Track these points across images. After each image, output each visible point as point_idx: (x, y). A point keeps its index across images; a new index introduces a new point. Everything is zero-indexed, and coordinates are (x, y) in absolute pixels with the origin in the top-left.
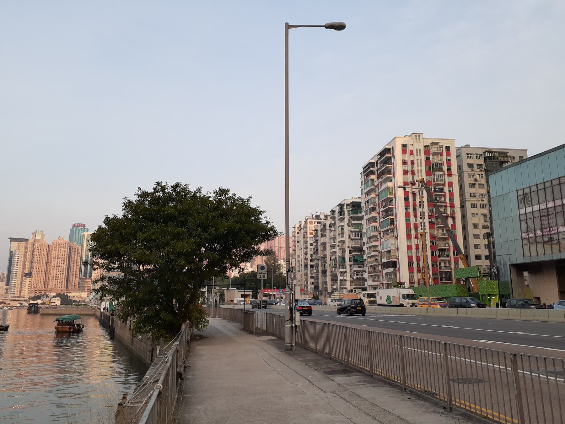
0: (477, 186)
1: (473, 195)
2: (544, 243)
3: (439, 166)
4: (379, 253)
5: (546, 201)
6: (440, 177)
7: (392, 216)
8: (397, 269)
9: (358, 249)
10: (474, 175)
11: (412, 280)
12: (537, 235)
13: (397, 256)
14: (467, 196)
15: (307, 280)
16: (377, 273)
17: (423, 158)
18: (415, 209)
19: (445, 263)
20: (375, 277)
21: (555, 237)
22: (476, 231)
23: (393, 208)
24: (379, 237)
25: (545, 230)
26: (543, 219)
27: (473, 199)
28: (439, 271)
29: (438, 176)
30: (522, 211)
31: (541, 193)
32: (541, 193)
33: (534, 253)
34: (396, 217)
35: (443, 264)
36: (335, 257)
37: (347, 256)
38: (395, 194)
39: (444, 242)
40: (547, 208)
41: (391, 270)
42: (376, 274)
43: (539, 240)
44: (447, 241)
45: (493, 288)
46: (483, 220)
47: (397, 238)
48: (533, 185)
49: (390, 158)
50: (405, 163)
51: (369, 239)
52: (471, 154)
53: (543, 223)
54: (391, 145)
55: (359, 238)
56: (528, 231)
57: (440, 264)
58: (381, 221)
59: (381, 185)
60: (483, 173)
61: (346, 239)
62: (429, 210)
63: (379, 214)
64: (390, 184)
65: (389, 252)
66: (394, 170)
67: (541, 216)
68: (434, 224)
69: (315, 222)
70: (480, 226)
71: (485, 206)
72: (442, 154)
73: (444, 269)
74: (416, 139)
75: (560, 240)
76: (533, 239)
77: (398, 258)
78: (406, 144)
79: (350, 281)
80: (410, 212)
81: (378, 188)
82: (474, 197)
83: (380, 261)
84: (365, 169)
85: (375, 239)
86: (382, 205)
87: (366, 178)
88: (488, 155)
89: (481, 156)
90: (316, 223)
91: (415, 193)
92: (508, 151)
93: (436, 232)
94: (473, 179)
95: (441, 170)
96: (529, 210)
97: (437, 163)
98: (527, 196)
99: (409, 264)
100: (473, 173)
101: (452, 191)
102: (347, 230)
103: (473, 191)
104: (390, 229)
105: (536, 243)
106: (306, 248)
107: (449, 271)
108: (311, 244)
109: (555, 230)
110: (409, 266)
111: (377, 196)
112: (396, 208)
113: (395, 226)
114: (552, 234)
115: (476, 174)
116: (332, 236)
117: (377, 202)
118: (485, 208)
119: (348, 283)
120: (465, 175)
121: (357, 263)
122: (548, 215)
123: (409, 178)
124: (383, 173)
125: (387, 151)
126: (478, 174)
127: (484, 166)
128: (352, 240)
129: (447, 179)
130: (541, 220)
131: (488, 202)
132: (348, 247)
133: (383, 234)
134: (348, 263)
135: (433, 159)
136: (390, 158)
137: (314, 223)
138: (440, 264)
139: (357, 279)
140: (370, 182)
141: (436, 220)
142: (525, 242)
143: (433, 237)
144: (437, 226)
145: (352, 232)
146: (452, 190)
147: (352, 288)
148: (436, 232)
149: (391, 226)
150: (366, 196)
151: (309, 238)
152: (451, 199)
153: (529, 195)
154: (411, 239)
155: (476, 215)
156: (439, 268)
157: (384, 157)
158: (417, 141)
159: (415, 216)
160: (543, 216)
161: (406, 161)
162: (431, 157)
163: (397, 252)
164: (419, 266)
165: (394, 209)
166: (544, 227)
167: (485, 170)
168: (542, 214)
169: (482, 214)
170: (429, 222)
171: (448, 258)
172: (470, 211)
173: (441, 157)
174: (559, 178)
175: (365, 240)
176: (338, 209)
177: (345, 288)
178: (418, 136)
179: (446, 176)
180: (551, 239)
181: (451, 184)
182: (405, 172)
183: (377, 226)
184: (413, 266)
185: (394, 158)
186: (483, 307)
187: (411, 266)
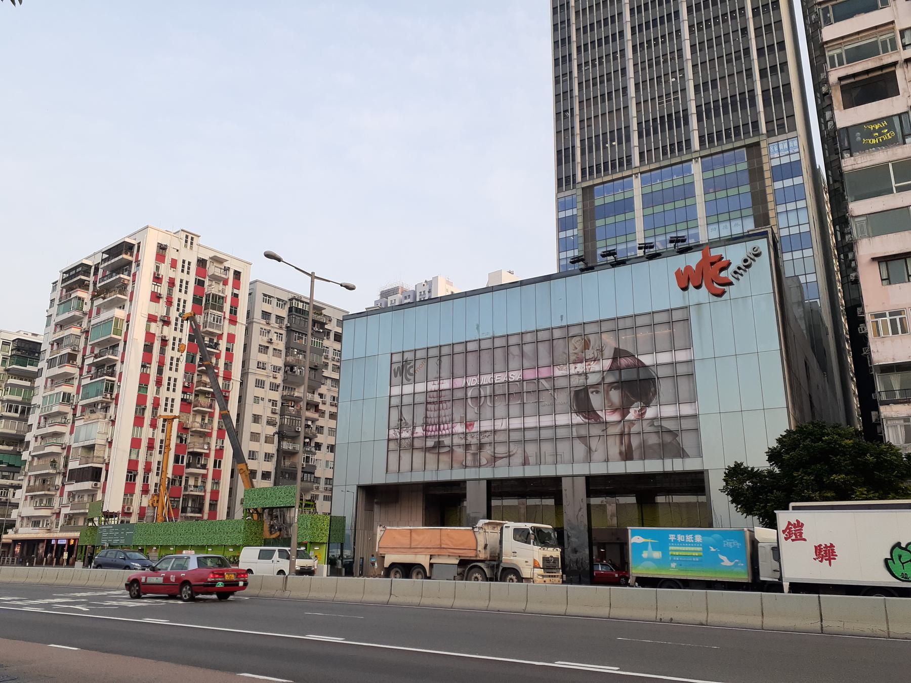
0: (270, 351)
1: (261, 366)
2: (426, 450)
3: (216, 302)
4: (63, 449)
5: (440, 377)
6: (217, 322)
7: (111, 376)
8: (100, 484)
9: (10, 439)
10: (268, 332)
11: (129, 509)
12: (415, 435)
13: (106, 457)
14: (253, 366)
16: (49, 490)
17: (192, 278)
18: (160, 371)
19: (196, 480)
20: (41, 501)
21: (447, 441)
22: (256, 428)
23: (117, 360)
24: (70, 417)
25: (431, 427)
26: (429, 409)
27: (260, 371)
28: (183, 493)
29: (214, 318)
30: (396, 391)
31: (433, 363)
32: (433, 363)
33: (405, 465)
34: (120, 380)
35: (191, 482)
38: (126, 333)
39: (201, 440)
40: (466, 387)
41: (88, 485)
42: (47, 492)
43: (417, 444)
44: (208, 440)
45: (322, 530)
46: (269, 411)
47: (113, 422)
48: (409, 349)
49: (130, 263)
50: (157, 279)
51: (45, 418)
52: (270, 297)
53: (428, 416)
54: (135, 239)
55: (17, 415)
56: (401, 426)
57: (187, 481)
58: (83, 384)
59: (98, 313)
60: (284, 332)
62: (185, 376)
63: (81, 369)
64: (119, 313)
65: (91, 448)
66: (133, 287)
67: (427, 403)
68: (190, 403)
70: (264, 420)
71: (278, 388)
72: (225, 283)
73: (191, 491)
74: (186, 242)
75: (453, 447)
76: (407, 441)
77: (107, 461)
78: (166, 246)
80: (149, 375)
81: (90, 317)
82: (263, 369)
83: (62, 467)
85: (59, 420)
86: (92, 352)
87: (64, 293)
88: (295, 304)
89: (285, 304)
91: (167, 341)
92: (324, 306)
93: (191, 420)
94: (266, 339)
95: (221, 309)
96: (408, 389)
97: (216, 295)
98: (408, 366)
99: (127, 476)
100: (268, 328)
101: (232, 351)
103: (262, 358)
104: (102, 402)
105: (413, 449)
107: (200, 496)
109: (448, 429)
110: (127, 480)
111: (83, 333)
112: (122, 362)
113: (114, 396)
114: (442, 435)
115: (273, 331)
117: (82, 346)
118: (277, 391)
120: (256, 328)
122: (440, 402)
123: (160, 309)
124: (107, 289)
126: (275, 333)
127: (286, 322)
129: (227, 328)
130: (426, 410)
131: (283, 381)
133: (83, 411)
135: (210, 286)
136: (130, 263)
138: (187, 481)
140: (74, 303)
141: (194, 399)
142: (392, 445)
143: (183, 428)
146: (232, 349)
148: (191, 420)
149: (106, 395)
150: (58, 330)
152: (228, 366)
153: (412, 364)
154: (142, 426)
156: (183, 489)
157: (117, 259)
158: (186, 246)
159: (159, 383)
160: (430, 403)
161: (160, 277)
162: (207, 283)
163: (107, 449)
164: (147, 482)
165: (119, 364)
166: (429, 422)
167: (287, 327)
168: (429, 400)
169: (270, 400)
170: (182, 400)
171: (203, 471)
172: (252, 391)
173: (224, 287)
174: (466, 342)
175: (33, 419)
178: (190, 239)
179: (227, 322)
180: (439, 445)
181: (231, 338)
182: (156, 297)
183: (69, 394)
184: (134, 480)
185: (138, 265)
186: (349, 572)
187: (131, 480)
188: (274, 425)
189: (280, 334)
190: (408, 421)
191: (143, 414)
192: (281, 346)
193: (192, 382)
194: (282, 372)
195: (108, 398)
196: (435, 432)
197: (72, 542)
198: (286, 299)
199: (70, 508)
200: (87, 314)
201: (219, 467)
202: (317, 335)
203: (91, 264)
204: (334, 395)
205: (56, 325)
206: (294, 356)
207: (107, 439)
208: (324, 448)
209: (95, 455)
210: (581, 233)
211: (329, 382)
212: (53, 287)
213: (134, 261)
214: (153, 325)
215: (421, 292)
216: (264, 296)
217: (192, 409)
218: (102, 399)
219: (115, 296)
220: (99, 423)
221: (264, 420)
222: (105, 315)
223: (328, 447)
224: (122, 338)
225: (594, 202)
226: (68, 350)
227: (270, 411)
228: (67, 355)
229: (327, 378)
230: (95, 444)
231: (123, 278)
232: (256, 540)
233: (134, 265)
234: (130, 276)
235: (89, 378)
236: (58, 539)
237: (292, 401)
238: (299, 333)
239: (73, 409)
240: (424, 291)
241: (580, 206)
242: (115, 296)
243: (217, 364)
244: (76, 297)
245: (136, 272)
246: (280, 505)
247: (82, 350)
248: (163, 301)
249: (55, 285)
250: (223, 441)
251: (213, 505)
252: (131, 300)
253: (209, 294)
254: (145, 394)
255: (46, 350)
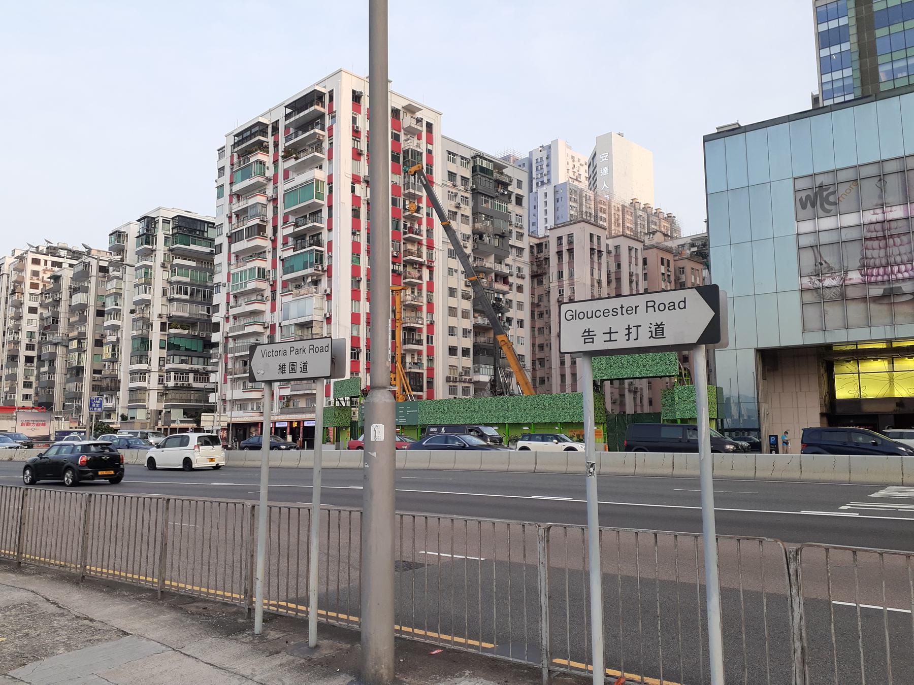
0: (459, 217)
4: (265, 328)
10: (456, 196)
15: (13, 390)
24: (268, 293)
35: (409, 359)
36: (115, 338)
37: (156, 336)
39: (413, 314)
44: (419, 314)
45: (563, 409)
47: (329, 296)
49: (322, 116)
52: (454, 155)
54: (325, 87)
55: (187, 297)
60: (469, 195)
61: (157, 298)
63: (274, 241)
64: (320, 175)
68: (399, 275)
69: (46, 261)
70: (459, 294)
76: (834, 290)
79: (157, 391)
84: (240, 138)
85: (254, 298)
90: (49, 263)
94: (453, 203)
97: (415, 150)
98: (825, 193)
99: (352, 353)
100: (455, 191)
102: (160, 277)
104: (312, 275)
106: (18, 318)
108: (33, 310)
112: (330, 230)
116: (114, 291)
117: (270, 215)
119: (153, 395)
121: (177, 352)
125: (314, 97)
128: (171, 300)
132: (160, 316)
134: (156, 353)
135: (406, 140)
136: (322, 116)
137: (42, 262)
139: (176, 388)
144: (407, 280)
145: (171, 283)
147: (161, 406)
149: (318, 267)
150: (235, 200)
151: (27, 296)
154: (359, 300)
155: (454, 272)
161: (359, 130)
162: (402, 137)
167: (473, 190)
176: (134, 230)
177: (144, 407)
184: (358, 358)
185: (333, 117)
187: (355, 358)
188: (468, 299)
189: (466, 198)
190: (832, 265)
191: (359, 287)
192: (467, 210)
193: (400, 251)
194: (471, 240)
195: (319, 270)
196: (883, 276)
197: (295, 425)
198: (469, 157)
199: (290, 389)
200: (271, 180)
201: (432, 343)
202: (502, 198)
203: (268, 123)
204: (520, 266)
205: (231, 196)
206: (482, 222)
207: (325, 315)
208: (514, 323)
209: (314, 332)
210: (855, 48)
211: (514, 251)
212: (219, 154)
213: (327, 113)
214: (357, 186)
215: (537, 159)
216: (448, 153)
217: (403, 281)
218: (313, 271)
219: (311, 155)
220: (314, 298)
221: (459, 294)
222: (299, 179)
223: (518, 322)
224: (325, 202)
225: (872, 7)
226: (256, 221)
227: (464, 284)
228: (256, 227)
229: (512, 246)
230: (312, 321)
231: (318, 134)
232: (565, 416)
233: (327, 117)
234: (324, 131)
235: (292, 250)
236: (275, 422)
237: (483, 272)
238: (486, 195)
239: (271, 285)
240: (541, 158)
241: (852, 13)
242: (311, 155)
243: (420, 229)
244: (257, 161)
245: (332, 126)
246: (647, 374)
247: (271, 222)
248: (364, 159)
249: (221, 151)
250: (432, 315)
251: (430, 383)
252: (330, 158)
253: (408, 150)
254: (358, 265)
255: (222, 224)
